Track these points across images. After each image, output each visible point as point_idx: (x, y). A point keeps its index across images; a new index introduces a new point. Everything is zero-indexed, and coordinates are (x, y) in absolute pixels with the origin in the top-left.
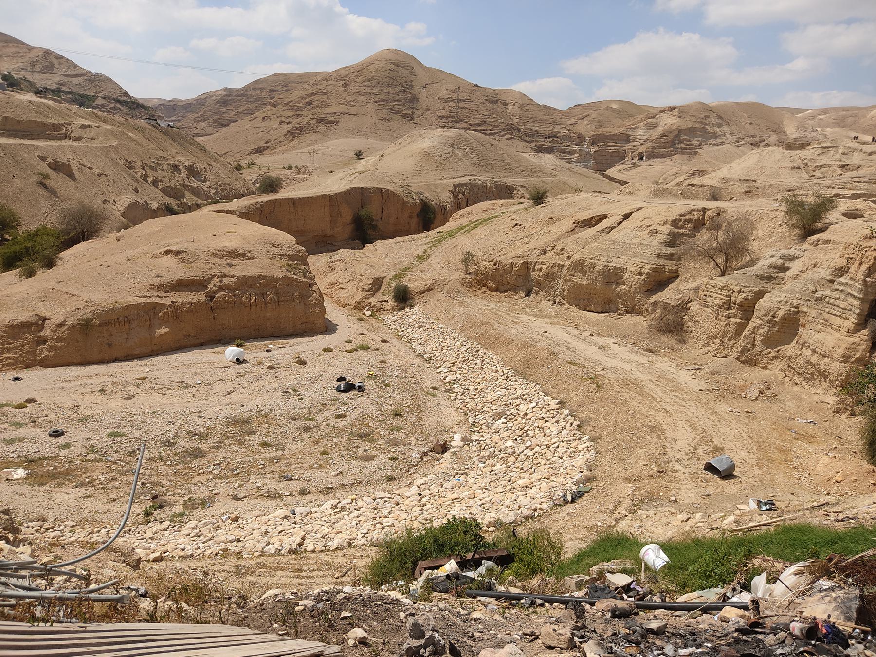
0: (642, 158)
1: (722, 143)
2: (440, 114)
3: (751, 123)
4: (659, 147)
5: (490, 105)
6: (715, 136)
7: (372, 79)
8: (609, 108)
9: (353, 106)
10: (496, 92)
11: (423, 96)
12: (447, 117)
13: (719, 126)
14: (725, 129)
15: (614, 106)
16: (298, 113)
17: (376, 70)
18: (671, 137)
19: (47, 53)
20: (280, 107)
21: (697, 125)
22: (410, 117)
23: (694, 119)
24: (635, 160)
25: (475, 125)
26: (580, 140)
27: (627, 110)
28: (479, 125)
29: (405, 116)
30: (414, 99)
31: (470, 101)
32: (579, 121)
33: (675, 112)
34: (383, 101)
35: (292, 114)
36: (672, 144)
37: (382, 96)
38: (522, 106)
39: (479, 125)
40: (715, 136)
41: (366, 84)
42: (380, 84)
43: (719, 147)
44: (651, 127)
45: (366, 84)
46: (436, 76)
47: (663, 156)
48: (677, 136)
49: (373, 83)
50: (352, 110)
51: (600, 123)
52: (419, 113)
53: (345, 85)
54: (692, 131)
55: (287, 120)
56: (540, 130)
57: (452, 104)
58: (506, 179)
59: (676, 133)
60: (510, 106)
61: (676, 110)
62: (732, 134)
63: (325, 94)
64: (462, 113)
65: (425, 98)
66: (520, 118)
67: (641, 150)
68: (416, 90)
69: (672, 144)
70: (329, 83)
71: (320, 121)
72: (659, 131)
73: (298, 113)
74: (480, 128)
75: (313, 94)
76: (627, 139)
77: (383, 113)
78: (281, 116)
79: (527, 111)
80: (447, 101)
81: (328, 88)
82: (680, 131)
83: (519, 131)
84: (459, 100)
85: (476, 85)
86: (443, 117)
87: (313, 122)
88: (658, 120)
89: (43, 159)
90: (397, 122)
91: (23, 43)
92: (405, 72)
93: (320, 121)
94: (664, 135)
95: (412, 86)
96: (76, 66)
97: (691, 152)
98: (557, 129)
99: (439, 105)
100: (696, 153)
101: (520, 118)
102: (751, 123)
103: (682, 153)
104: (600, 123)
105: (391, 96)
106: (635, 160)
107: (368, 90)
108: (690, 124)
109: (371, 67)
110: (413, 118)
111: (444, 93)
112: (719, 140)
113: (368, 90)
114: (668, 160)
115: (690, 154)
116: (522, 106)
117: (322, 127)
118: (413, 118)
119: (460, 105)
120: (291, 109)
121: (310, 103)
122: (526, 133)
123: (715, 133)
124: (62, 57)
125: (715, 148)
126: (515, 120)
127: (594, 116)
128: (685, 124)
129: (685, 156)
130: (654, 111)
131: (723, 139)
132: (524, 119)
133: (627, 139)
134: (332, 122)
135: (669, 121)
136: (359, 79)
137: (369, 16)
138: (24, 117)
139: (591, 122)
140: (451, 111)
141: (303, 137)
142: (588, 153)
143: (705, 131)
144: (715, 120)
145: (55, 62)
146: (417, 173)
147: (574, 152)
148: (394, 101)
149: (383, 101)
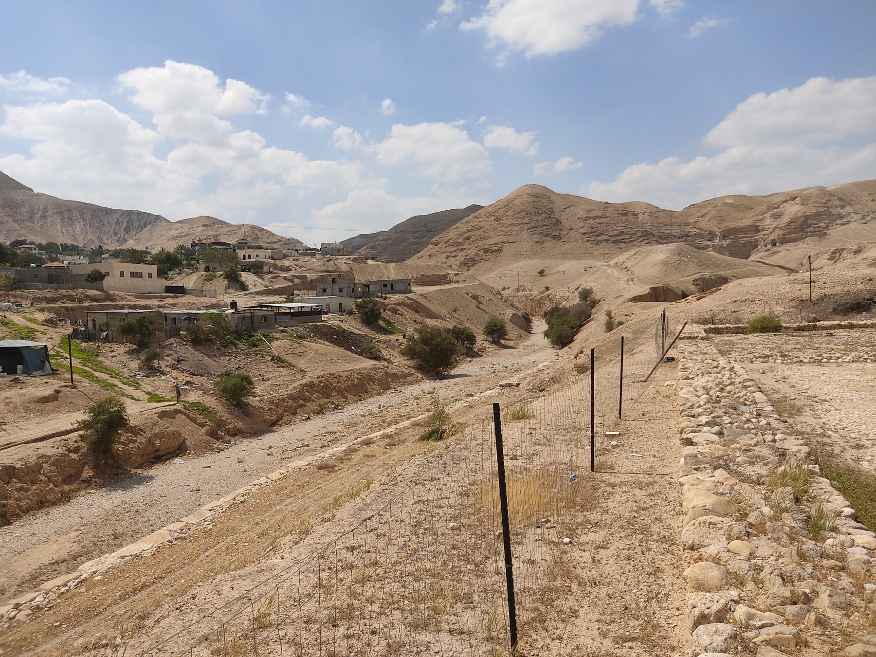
0: (775, 245)
1: (848, 223)
2: (582, 231)
3: (873, 200)
4: (790, 233)
5: (624, 218)
6: (841, 217)
7: (521, 211)
8: (725, 204)
9: (510, 235)
10: (624, 206)
11: (564, 218)
12: (589, 233)
13: (842, 207)
14: (848, 209)
15: (729, 201)
16: (460, 247)
17: (523, 204)
18: (799, 223)
19: (253, 227)
20: (441, 244)
21: (821, 210)
22: (558, 238)
23: (816, 205)
24: (769, 247)
25: (615, 236)
26: (712, 236)
27: (743, 204)
28: (618, 235)
29: (554, 237)
30: (558, 222)
31: (605, 217)
33: (798, 200)
34: (534, 227)
35: (454, 249)
36: (802, 229)
37: (533, 224)
38: (651, 215)
39: (618, 235)
40: (841, 217)
41: (517, 216)
42: (529, 214)
43: (846, 226)
44: (777, 216)
45: (517, 216)
46: (571, 201)
47: (794, 240)
48: (804, 221)
49: (523, 214)
50: (511, 239)
51: (721, 219)
52: (564, 233)
53: (497, 220)
54: (817, 215)
55: (453, 254)
57: (591, 221)
58: (720, 273)
59: (802, 219)
60: (640, 216)
61: (798, 199)
62: (857, 213)
63: (480, 229)
64: (602, 228)
65: (566, 222)
66: (652, 225)
67: (772, 237)
68: (557, 214)
69: (802, 229)
70: (480, 219)
71: (486, 251)
72: (785, 219)
73: (460, 247)
74: (619, 238)
75: (468, 231)
76: (756, 229)
77: (537, 238)
78: (445, 252)
79: (657, 217)
80: (586, 219)
81: (481, 224)
82: (806, 217)
83: (654, 235)
84: (596, 218)
85: (607, 203)
86: (585, 234)
87: (482, 253)
88: (783, 210)
89: (468, 294)
90: (549, 244)
91: (225, 223)
92: (545, 202)
93: (486, 251)
94: (791, 222)
95: (553, 212)
96: (273, 234)
97: (821, 234)
98: (687, 229)
99: (579, 224)
100: (825, 234)
101: (652, 225)
102: (873, 200)
103: (812, 236)
104: (721, 219)
105: (540, 223)
106: (769, 247)
107: (520, 221)
108: (814, 210)
109: (515, 202)
110: (561, 238)
111: (581, 214)
112: (844, 220)
113: (520, 221)
114: (800, 243)
115: (820, 236)
116: (651, 215)
117: (489, 256)
118: (561, 238)
119: (597, 221)
120: (453, 245)
121: (468, 238)
122: (660, 237)
123: (839, 214)
124: (263, 229)
125: (842, 228)
126: (648, 227)
127: (713, 213)
128: (810, 210)
129: (816, 238)
130: (776, 200)
131: (849, 218)
132: (655, 225)
133: (756, 229)
134: (497, 251)
135: (793, 210)
136: (510, 213)
137: (247, 83)
138: (430, 273)
139: (712, 219)
140: (591, 228)
141: (477, 266)
142: (722, 246)
143: (830, 214)
145: (259, 234)
146: (666, 276)
147: (708, 247)
148: (543, 226)
149: (534, 227)
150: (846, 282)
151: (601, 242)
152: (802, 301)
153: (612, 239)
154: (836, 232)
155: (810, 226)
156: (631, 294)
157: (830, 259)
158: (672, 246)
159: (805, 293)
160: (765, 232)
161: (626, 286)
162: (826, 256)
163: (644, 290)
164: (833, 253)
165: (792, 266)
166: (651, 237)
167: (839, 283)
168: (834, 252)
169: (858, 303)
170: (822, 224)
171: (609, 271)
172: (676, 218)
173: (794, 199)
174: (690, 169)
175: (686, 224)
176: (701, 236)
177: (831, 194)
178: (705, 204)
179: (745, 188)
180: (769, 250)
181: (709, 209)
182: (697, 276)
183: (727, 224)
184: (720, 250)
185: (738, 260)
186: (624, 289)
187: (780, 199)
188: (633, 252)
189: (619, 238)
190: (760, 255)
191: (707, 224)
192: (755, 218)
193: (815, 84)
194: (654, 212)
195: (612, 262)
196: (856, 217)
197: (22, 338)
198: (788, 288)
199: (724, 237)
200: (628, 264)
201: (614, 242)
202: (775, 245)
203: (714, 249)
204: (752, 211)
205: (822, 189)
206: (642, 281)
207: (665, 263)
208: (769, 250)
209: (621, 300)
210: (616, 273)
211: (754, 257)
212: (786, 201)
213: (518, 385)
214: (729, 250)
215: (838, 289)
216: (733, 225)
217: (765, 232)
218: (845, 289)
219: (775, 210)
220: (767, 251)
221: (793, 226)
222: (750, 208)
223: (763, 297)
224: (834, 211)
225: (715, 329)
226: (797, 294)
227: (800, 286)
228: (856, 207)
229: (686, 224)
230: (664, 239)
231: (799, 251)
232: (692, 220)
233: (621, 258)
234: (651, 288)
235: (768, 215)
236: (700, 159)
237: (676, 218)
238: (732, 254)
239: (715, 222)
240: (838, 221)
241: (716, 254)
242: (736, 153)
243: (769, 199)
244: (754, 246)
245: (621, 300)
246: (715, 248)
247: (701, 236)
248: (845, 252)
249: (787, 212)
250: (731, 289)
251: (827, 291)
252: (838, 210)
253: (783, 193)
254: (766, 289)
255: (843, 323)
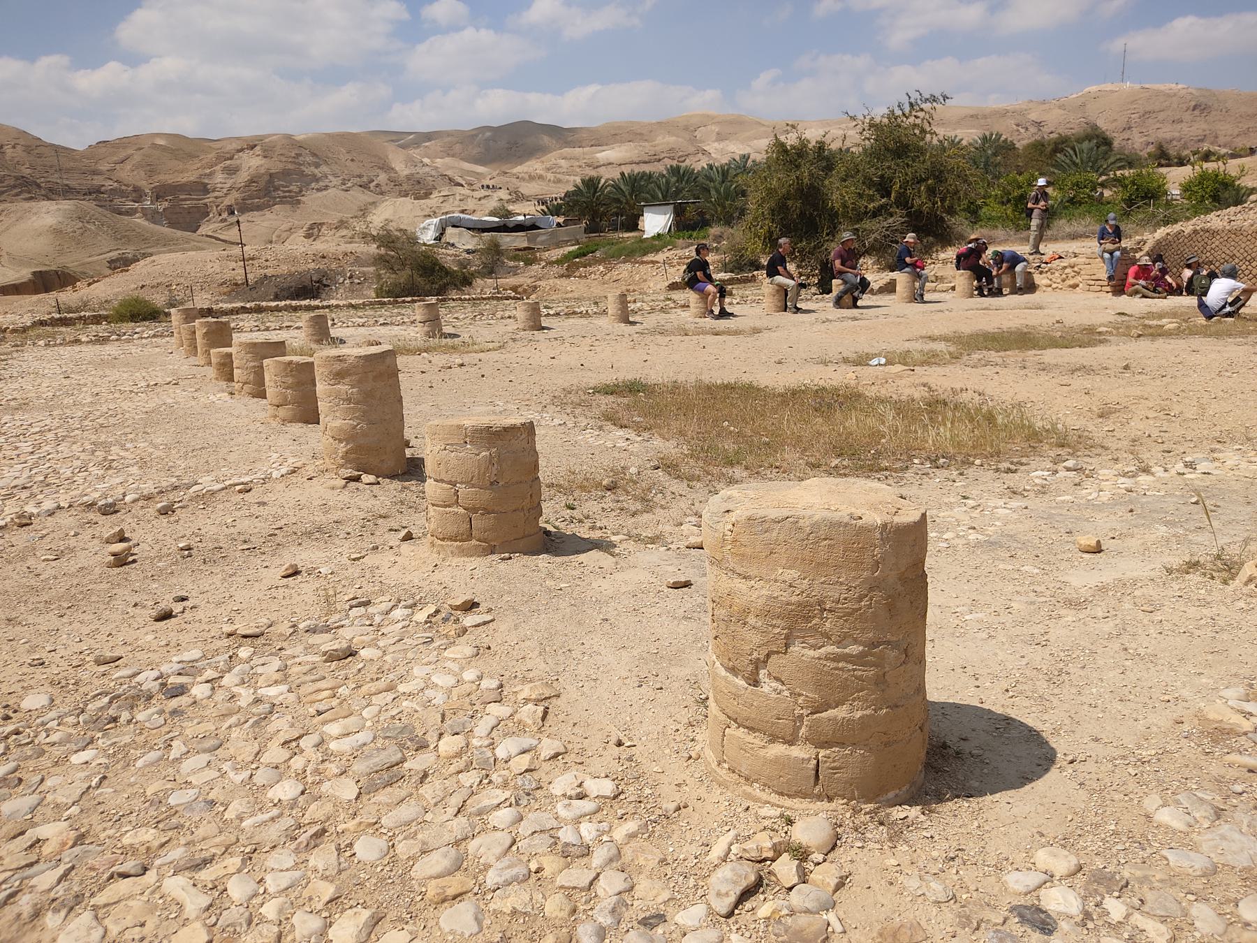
0: (233, 213)
1: (326, 188)
4: (251, 197)
8: (154, 146)
13: (317, 166)
14: (324, 169)
15: (161, 142)
18: (262, 184)
21: (290, 166)
26: (138, 194)
27: (181, 148)
32: (118, 167)
38: (28, 149)
43: (325, 193)
47: (259, 208)
54: (285, 174)
56: (72, 183)
59: (267, 178)
61: (258, 148)
62: (336, 176)
66: (32, 167)
67: (228, 201)
72: (243, 177)
76: (202, 188)
79: (40, 156)
82: (271, 175)
83: (39, 186)
88: (238, 162)
94: (252, 181)
97: (293, 201)
98: (98, 181)
100: (299, 202)
103: (281, 203)
106: (225, 215)
108: (281, 166)
112: (321, 184)
114: (266, 212)
116: (28, 149)
125: (320, 194)
126: (26, 172)
127: (137, 157)
128: (275, 166)
129: (288, 207)
131: (326, 182)
132: (39, 168)
135: (252, 163)
139: (137, 167)
142: (156, 212)
143: (302, 174)
144: (309, 159)
150: (294, 260)
152: (236, 284)
154: (312, 199)
155: (276, 189)
157: (308, 236)
158: (66, 205)
159: (239, 276)
160: (216, 194)
162: (301, 233)
164: (310, 229)
166: (34, 189)
167: (285, 261)
168: (311, 228)
169: (305, 287)
170: (294, 188)
172: (75, 160)
173: (253, 147)
174: (92, 81)
175: (95, 173)
176: (123, 194)
177: (300, 145)
178: (123, 143)
179: (189, 126)
180: (225, 220)
181: (130, 151)
182: (114, 255)
183: (162, 177)
184: (153, 217)
185: (179, 233)
187: (235, 146)
191: (128, 174)
193: (592, 89)
194: (34, 146)
196: (335, 181)
198: (217, 268)
199: (159, 195)
203: (145, 215)
204: (196, 161)
205: (289, 137)
206: (17, 261)
207: (57, 232)
208: (225, 220)
211: (205, 229)
212: (242, 150)
214: (167, 219)
215: (284, 269)
216: (169, 179)
217: (216, 194)
218: (293, 269)
219: (228, 162)
220: (222, 221)
221: (254, 187)
222: (192, 156)
223: (182, 280)
224: (309, 170)
225: (60, 319)
226: (228, 275)
227: (233, 265)
229: (95, 173)
230: (52, 193)
231: (266, 224)
232: (104, 167)
234: (34, 273)
235: (218, 168)
236: (113, 65)
237: (75, 160)
238: (172, 225)
239: (142, 173)
240: (313, 185)
241: (146, 223)
242: (169, 65)
243: (218, 145)
244: (204, 213)
246: (145, 213)
247: (123, 194)
248: (325, 227)
249: (245, 166)
250: (140, 269)
251: (269, 272)
254: (188, 268)
255: (248, 306)
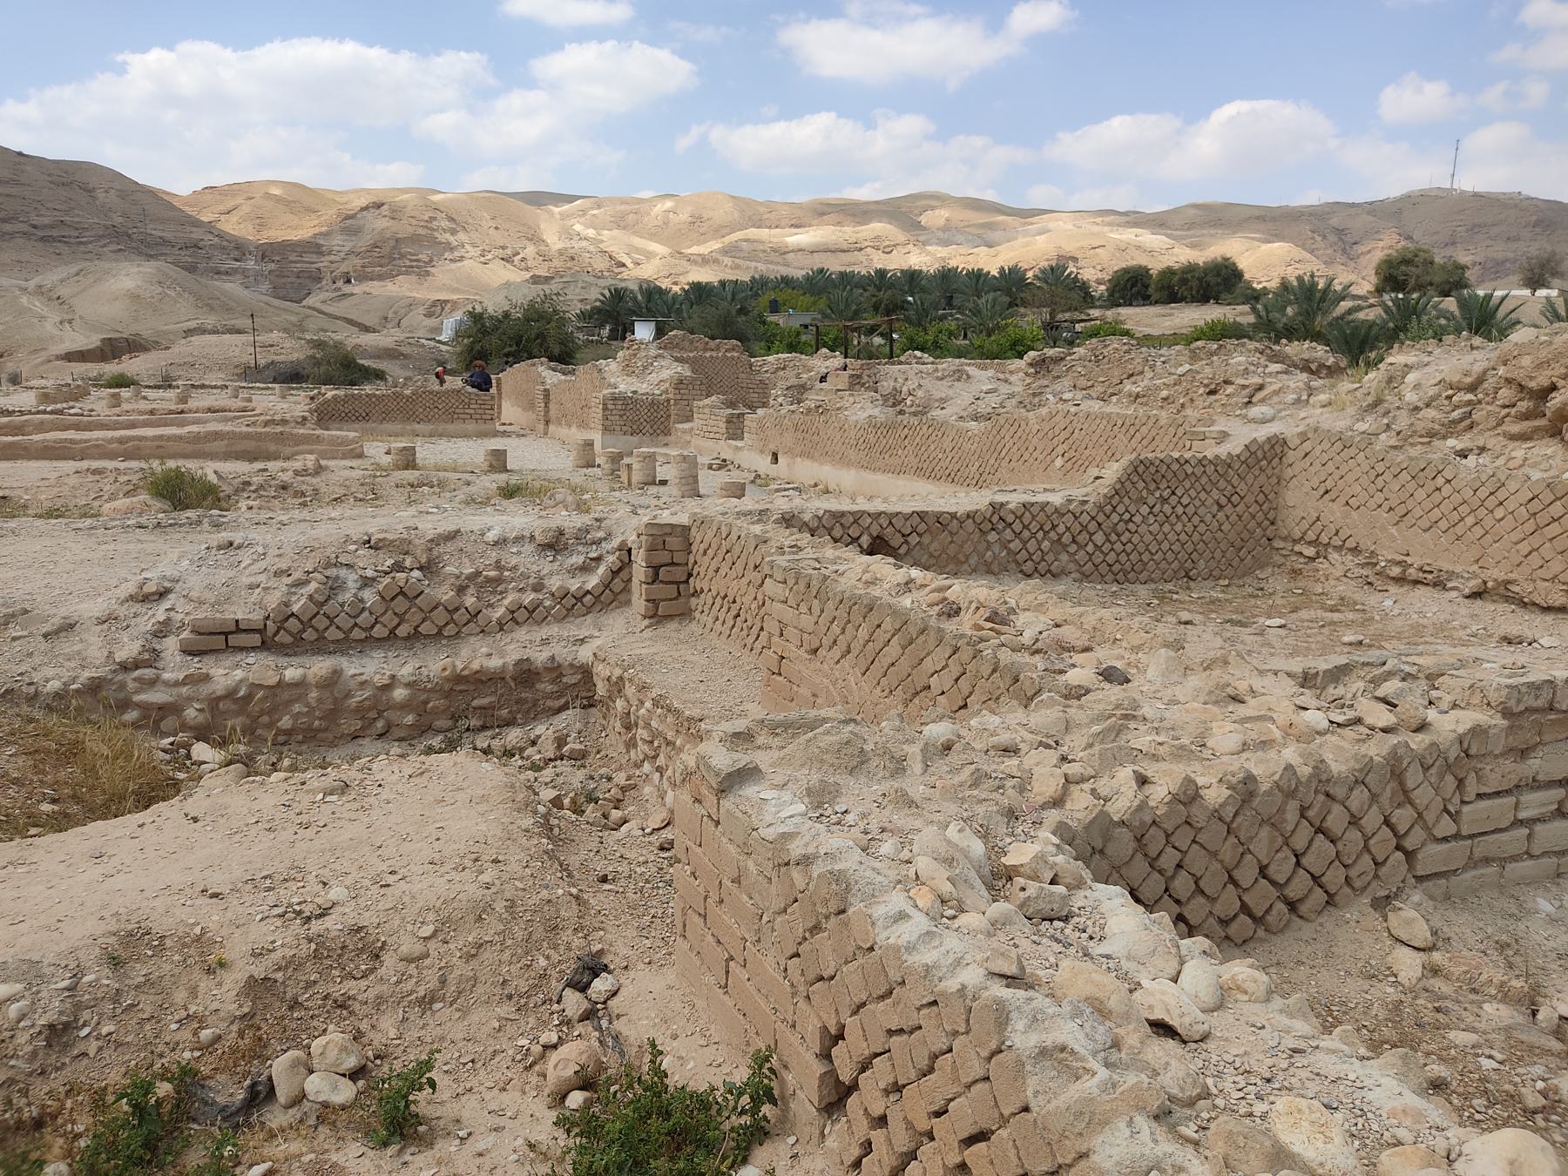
0: (349, 281)
4: (372, 265)
8: (268, 196)
13: (453, 232)
14: (462, 236)
15: (276, 191)
18: (386, 250)
21: (421, 231)
24: (340, 283)
25: (45, 227)
31: (18, 183)
39: (52, 227)
59: (392, 243)
66: (125, 215)
67: (344, 268)
72: (363, 242)
82: (397, 240)
85: (20, 154)
100: (428, 273)
103: (407, 273)
106: (340, 283)
108: (410, 230)
112: (457, 254)
125: (453, 266)
126: (118, 220)
127: (246, 209)
129: (414, 278)
143: (434, 242)
151: (12, 235)
153: (40, 234)
155: (402, 256)
156: (62, 348)
161: (56, 332)
163: (92, 341)
165: (369, 320)
171: (24, 300)
181: (239, 200)
186: (52, 338)
188: (74, 269)
189: (55, 233)
190: (323, 296)
192: (317, 230)
195: (32, 284)
197: (931, 476)
200: (64, 291)
201: (42, 239)
202: (349, 281)
207: (135, 297)
209: (43, 356)
210: (38, 305)
213: (832, 978)
228: (474, 235)
230: (147, 248)
233: (50, 278)
245: (43, 356)
252: (448, 235)
253: (368, 191)
